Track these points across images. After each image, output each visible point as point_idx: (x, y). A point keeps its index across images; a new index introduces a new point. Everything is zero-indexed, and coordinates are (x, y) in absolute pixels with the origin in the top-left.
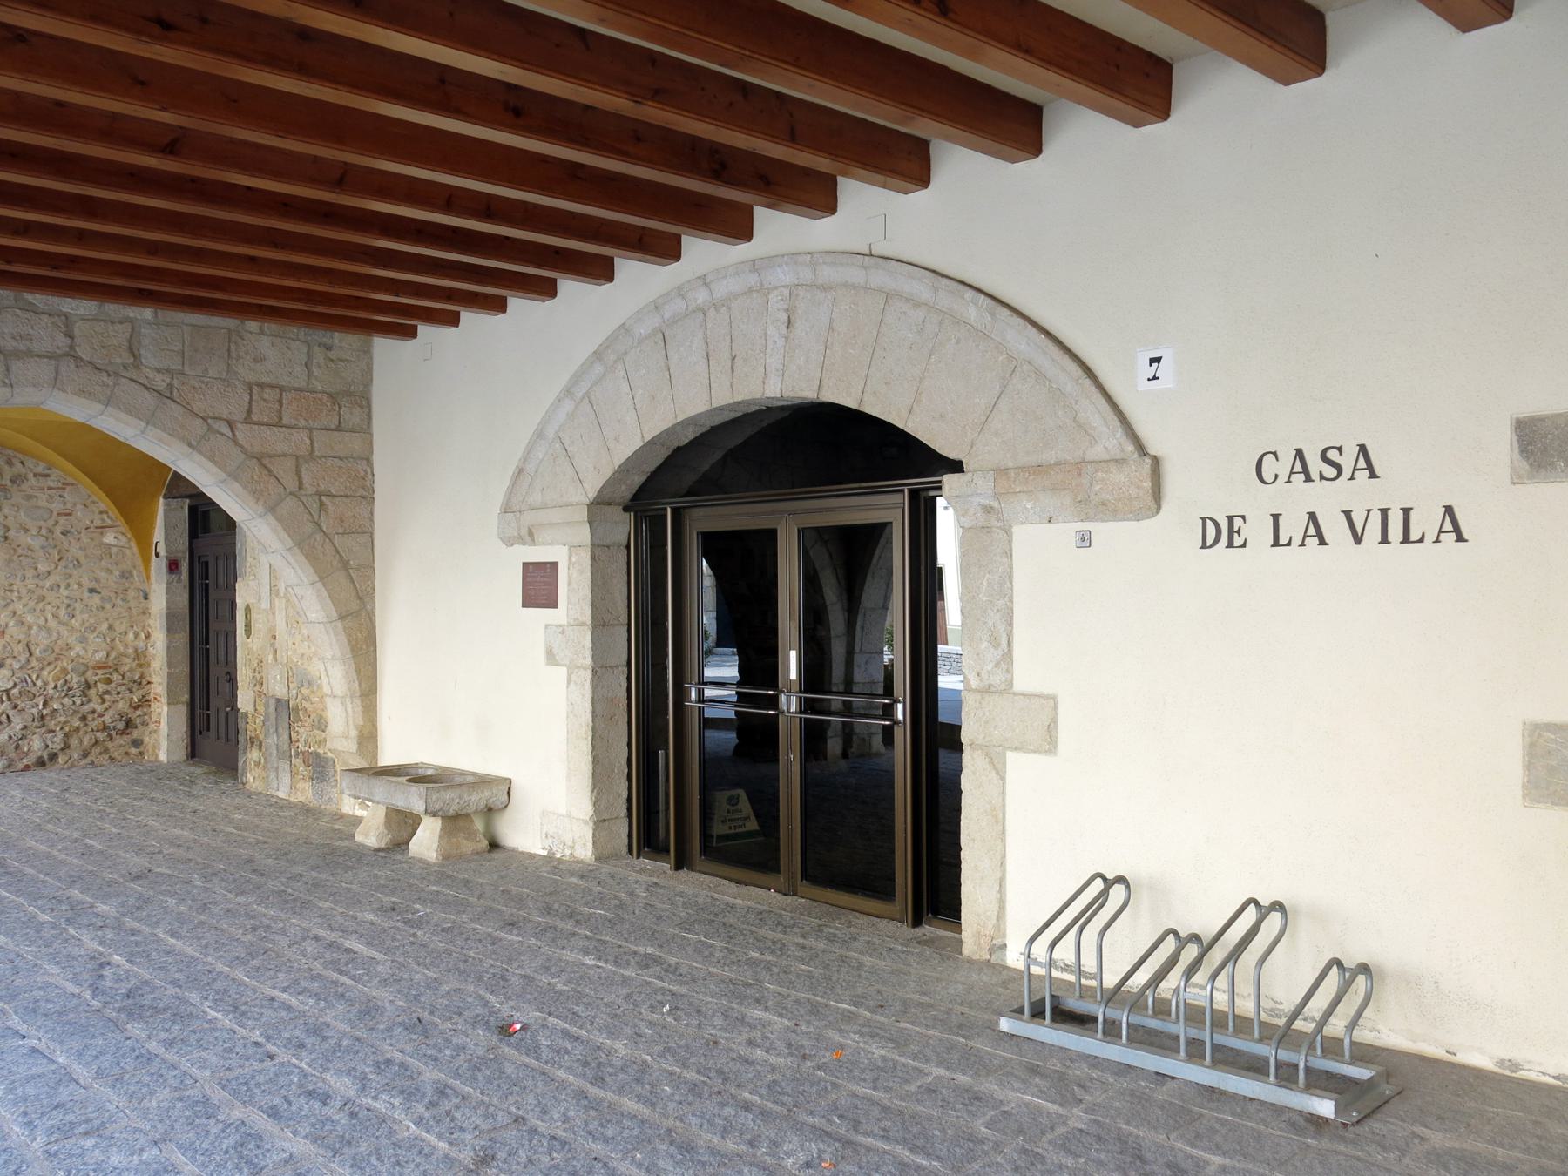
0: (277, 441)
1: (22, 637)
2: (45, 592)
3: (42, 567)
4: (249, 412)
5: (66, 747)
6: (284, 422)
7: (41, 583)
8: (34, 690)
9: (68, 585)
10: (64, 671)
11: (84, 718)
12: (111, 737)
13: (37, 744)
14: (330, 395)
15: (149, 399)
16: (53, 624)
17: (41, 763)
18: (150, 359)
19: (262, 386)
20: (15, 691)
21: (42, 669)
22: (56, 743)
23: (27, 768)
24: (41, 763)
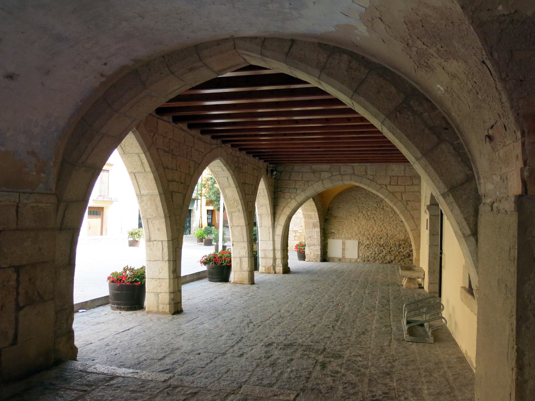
0: (396, 189)
1: (386, 232)
2: (391, 222)
3: (391, 216)
4: (390, 182)
5: (395, 259)
6: (399, 184)
7: (390, 219)
8: (388, 245)
9: (396, 220)
10: (395, 240)
11: (399, 253)
12: (405, 258)
13: (388, 258)
14: (410, 177)
15: (369, 182)
16: (392, 229)
17: (389, 262)
18: (369, 173)
19: (393, 176)
20: (384, 245)
21: (390, 240)
22: (393, 258)
23: (386, 263)
24: (389, 262)
